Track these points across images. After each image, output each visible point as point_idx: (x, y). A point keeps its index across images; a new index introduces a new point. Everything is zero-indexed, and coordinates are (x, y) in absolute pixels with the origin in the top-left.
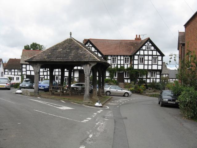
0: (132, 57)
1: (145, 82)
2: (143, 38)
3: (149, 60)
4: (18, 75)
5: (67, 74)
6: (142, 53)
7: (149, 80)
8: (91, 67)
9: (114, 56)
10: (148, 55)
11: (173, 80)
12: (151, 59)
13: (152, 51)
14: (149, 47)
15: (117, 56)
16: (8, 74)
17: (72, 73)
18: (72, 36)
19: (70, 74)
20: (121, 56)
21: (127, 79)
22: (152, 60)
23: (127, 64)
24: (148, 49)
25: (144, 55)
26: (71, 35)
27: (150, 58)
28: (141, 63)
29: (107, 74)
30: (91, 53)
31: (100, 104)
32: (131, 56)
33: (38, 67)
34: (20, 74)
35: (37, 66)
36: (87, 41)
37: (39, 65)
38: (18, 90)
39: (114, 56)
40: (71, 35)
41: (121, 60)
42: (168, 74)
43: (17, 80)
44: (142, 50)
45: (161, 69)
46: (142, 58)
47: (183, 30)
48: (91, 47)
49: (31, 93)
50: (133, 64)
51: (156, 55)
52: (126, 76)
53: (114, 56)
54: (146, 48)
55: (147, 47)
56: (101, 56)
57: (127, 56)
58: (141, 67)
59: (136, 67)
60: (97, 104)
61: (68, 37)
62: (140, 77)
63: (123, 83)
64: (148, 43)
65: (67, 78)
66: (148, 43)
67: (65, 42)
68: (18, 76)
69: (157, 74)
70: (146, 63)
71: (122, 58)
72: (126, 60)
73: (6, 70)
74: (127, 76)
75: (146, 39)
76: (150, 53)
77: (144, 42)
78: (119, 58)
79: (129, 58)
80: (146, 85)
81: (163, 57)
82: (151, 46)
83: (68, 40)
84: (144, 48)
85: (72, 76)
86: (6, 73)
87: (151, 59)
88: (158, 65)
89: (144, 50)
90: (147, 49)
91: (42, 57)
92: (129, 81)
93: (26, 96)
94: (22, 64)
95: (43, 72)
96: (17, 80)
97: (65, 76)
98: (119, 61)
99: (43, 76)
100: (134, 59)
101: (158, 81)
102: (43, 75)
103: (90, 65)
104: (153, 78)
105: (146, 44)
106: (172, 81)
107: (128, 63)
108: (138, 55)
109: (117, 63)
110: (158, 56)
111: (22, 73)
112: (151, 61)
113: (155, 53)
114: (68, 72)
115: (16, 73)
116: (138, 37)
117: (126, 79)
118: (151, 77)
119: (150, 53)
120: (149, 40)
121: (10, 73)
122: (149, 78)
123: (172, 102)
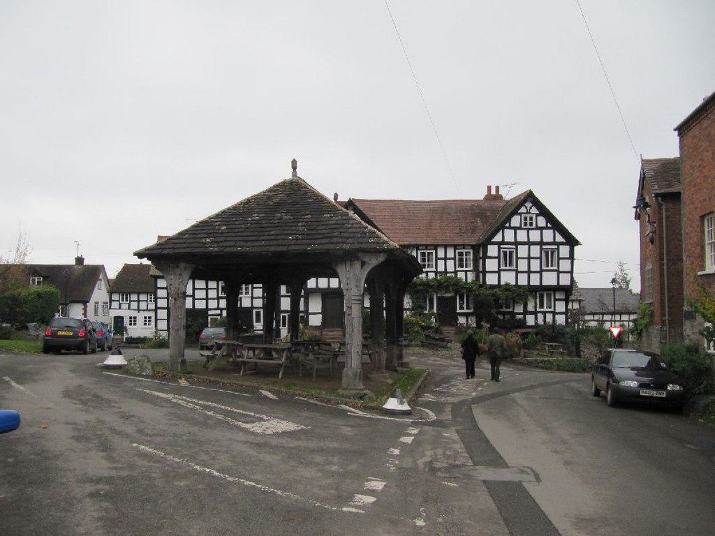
0: (479, 250)
1: (522, 323)
2: (509, 194)
3: (533, 258)
4: (147, 310)
5: (285, 304)
6: (509, 235)
7: (533, 316)
8: (367, 269)
9: (426, 249)
10: (529, 243)
11: (596, 317)
12: (539, 256)
14: (531, 219)
15: (436, 247)
16: (120, 308)
17: (302, 300)
18: (301, 173)
19: (295, 304)
20: (446, 247)
21: (467, 315)
22: (540, 258)
23: (466, 272)
24: (527, 226)
25: (517, 243)
26: (294, 168)
27: (535, 251)
28: (508, 268)
29: (407, 302)
30: (364, 224)
31: (402, 403)
32: (475, 248)
33: (184, 274)
34: (152, 306)
35: (178, 271)
36: (351, 204)
37: (185, 268)
38: (113, 354)
39: (426, 246)
40: (294, 168)
41: (445, 259)
42: (580, 301)
43: (145, 324)
44: (510, 228)
45: (568, 283)
46: (511, 253)
47: (670, 148)
48: (534, 217)
49: (155, 365)
50: (485, 272)
51: (554, 243)
52: (461, 308)
53: (426, 246)
54: (523, 221)
55: (526, 218)
56: (563, 240)
57: (464, 246)
58: (508, 278)
59: (491, 280)
60: (392, 404)
61: (288, 176)
62: (504, 310)
63: (454, 328)
64: (526, 208)
65: (286, 315)
66: (526, 208)
67: (274, 190)
68: (148, 314)
69: (556, 300)
70: (523, 265)
71: (450, 253)
72: (461, 260)
73: (115, 297)
74: (465, 306)
75: (522, 195)
76: (535, 235)
77: (517, 204)
78: (441, 253)
79: (471, 251)
80: (524, 336)
81: (576, 248)
82: (537, 215)
83: (284, 183)
84: (516, 221)
85: (302, 308)
86: (115, 305)
87: (539, 256)
88: (559, 272)
89: (515, 229)
90: (526, 224)
91: (197, 240)
92: (472, 321)
93: (140, 375)
94: (156, 277)
95: (218, 298)
96: (145, 324)
97: (282, 309)
98: (441, 264)
99: (218, 312)
100: (485, 257)
101: (561, 320)
102: (218, 308)
103: (363, 264)
104: (544, 313)
105: (523, 210)
106: (593, 320)
107: (467, 269)
108: (499, 244)
109: (434, 269)
110: (559, 244)
111: (156, 301)
112: (560, 256)
113: (548, 235)
114: (289, 299)
115: (143, 305)
116: (493, 192)
117: (461, 314)
118: (538, 310)
119: (535, 235)
120: (530, 197)
121: (125, 306)
122: (531, 313)
123: (654, 393)
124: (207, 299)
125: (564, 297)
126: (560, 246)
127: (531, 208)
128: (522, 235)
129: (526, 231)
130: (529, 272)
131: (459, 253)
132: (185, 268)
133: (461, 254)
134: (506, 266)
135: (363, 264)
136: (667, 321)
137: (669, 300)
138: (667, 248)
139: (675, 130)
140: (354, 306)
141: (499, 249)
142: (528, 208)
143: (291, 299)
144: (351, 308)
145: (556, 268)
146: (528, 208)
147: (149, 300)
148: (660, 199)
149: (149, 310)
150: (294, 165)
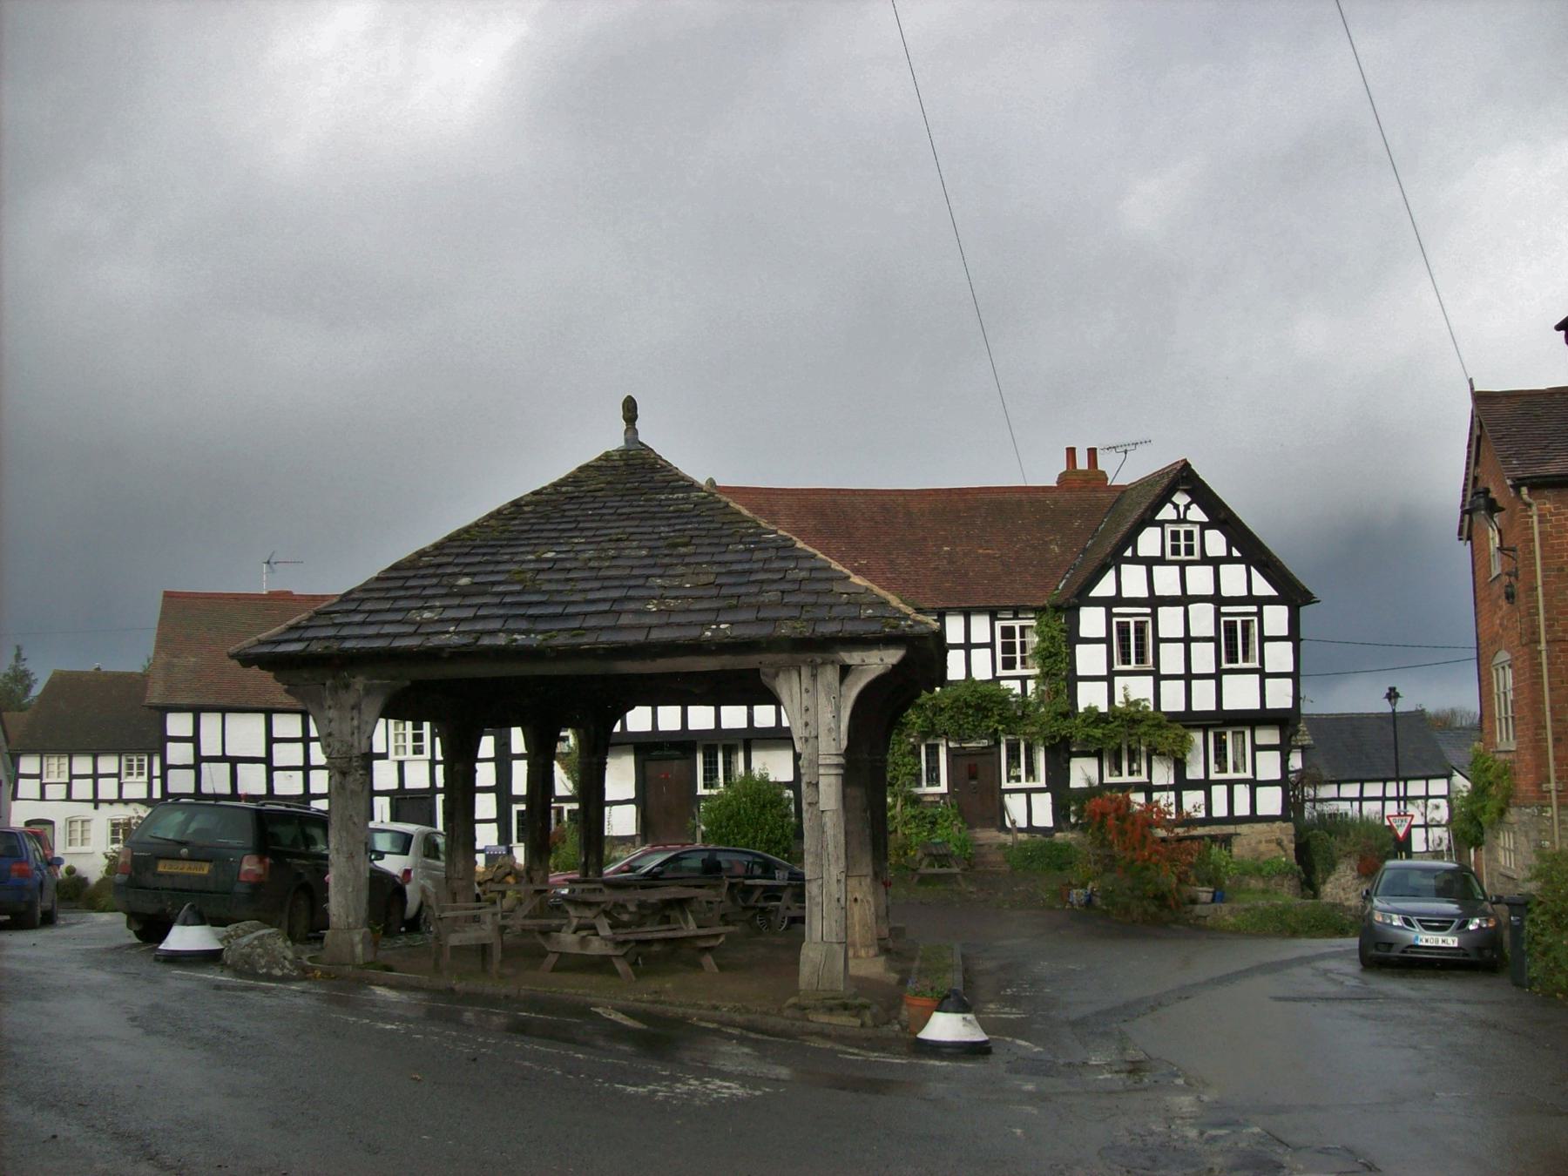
4: (121, 800)
6: (1133, 581)
13: (1215, 562)
14: (1189, 535)
16: (43, 798)
24: (1183, 554)
25: (1155, 602)
35: (349, 698)
37: (368, 691)
41: (968, 646)
44: (1136, 560)
45: (1287, 703)
46: (1140, 628)
48: (1196, 530)
51: (1249, 599)
54: (1168, 543)
55: (1175, 535)
56: (1272, 592)
59: (1091, 697)
61: (613, 439)
64: (1176, 507)
66: (1176, 507)
69: (1256, 748)
70: (1171, 659)
72: (1008, 648)
76: (1200, 580)
82: (1204, 527)
83: (607, 457)
84: (1149, 542)
88: (1263, 675)
89: (1150, 562)
90: (1176, 551)
93: (269, 977)
103: (845, 671)
104: (1230, 784)
105: (1167, 513)
108: (1108, 603)
110: (1262, 601)
113: (1234, 579)
115: (108, 788)
116: (1082, 463)
118: (1213, 776)
120: (1183, 478)
124: (307, 768)
125: (1277, 742)
126: (1266, 609)
127: (1187, 507)
128: (1167, 580)
129: (1176, 569)
130: (1188, 677)
131: (1003, 629)
132: (368, 691)
133: (1008, 632)
134: (1126, 661)
135: (845, 671)
136: (1554, 794)
137: (1557, 740)
138: (1547, 611)
139: (1558, 328)
140: (823, 782)
141: (1109, 616)
142: (1182, 509)
143: (529, 765)
144: (817, 784)
145: (1256, 665)
146: (1182, 509)
147: (124, 771)
148: (1524, 490)
149: (127, 802)
150: (630, 410)
